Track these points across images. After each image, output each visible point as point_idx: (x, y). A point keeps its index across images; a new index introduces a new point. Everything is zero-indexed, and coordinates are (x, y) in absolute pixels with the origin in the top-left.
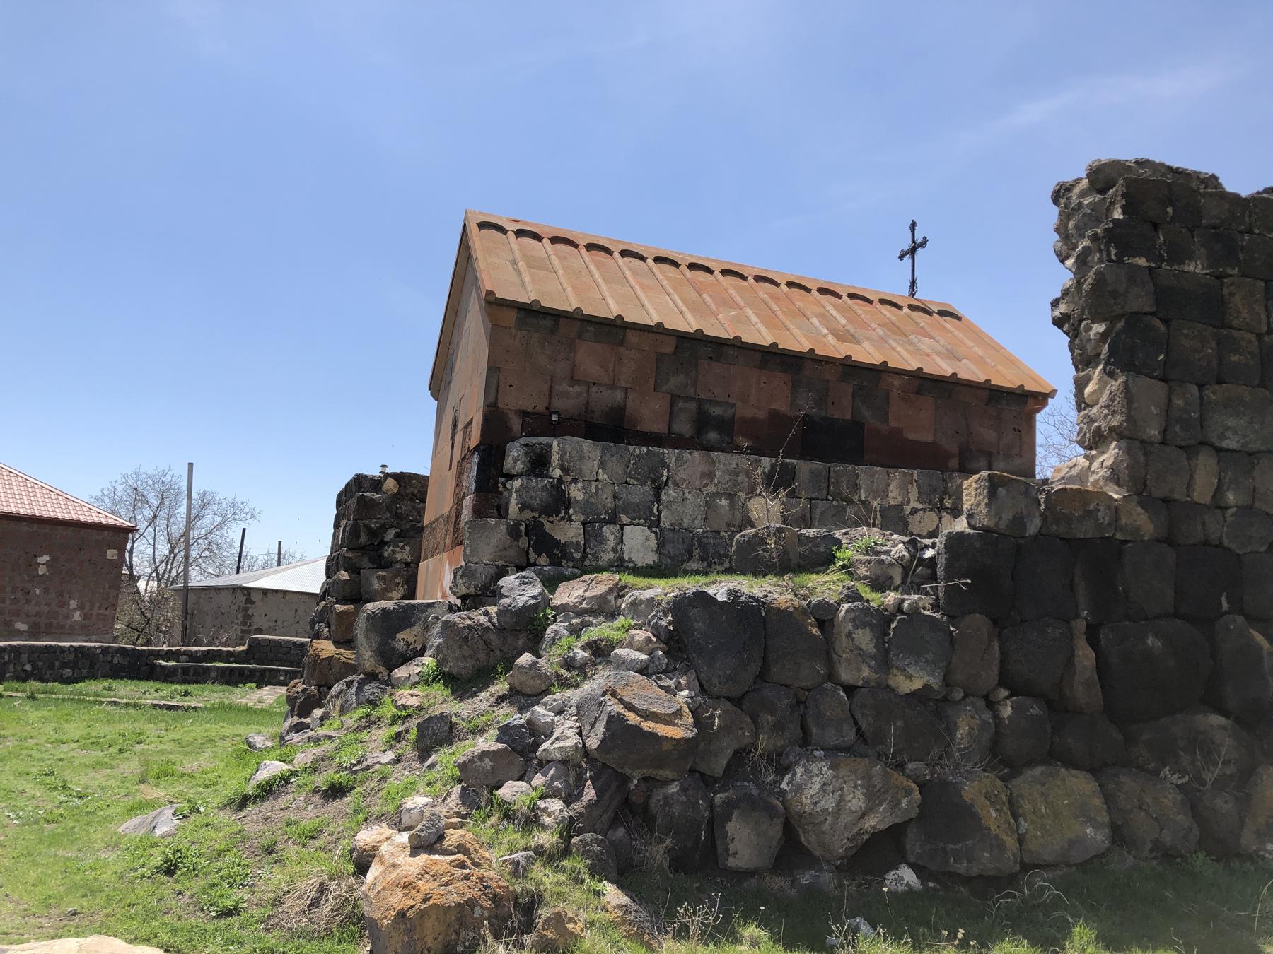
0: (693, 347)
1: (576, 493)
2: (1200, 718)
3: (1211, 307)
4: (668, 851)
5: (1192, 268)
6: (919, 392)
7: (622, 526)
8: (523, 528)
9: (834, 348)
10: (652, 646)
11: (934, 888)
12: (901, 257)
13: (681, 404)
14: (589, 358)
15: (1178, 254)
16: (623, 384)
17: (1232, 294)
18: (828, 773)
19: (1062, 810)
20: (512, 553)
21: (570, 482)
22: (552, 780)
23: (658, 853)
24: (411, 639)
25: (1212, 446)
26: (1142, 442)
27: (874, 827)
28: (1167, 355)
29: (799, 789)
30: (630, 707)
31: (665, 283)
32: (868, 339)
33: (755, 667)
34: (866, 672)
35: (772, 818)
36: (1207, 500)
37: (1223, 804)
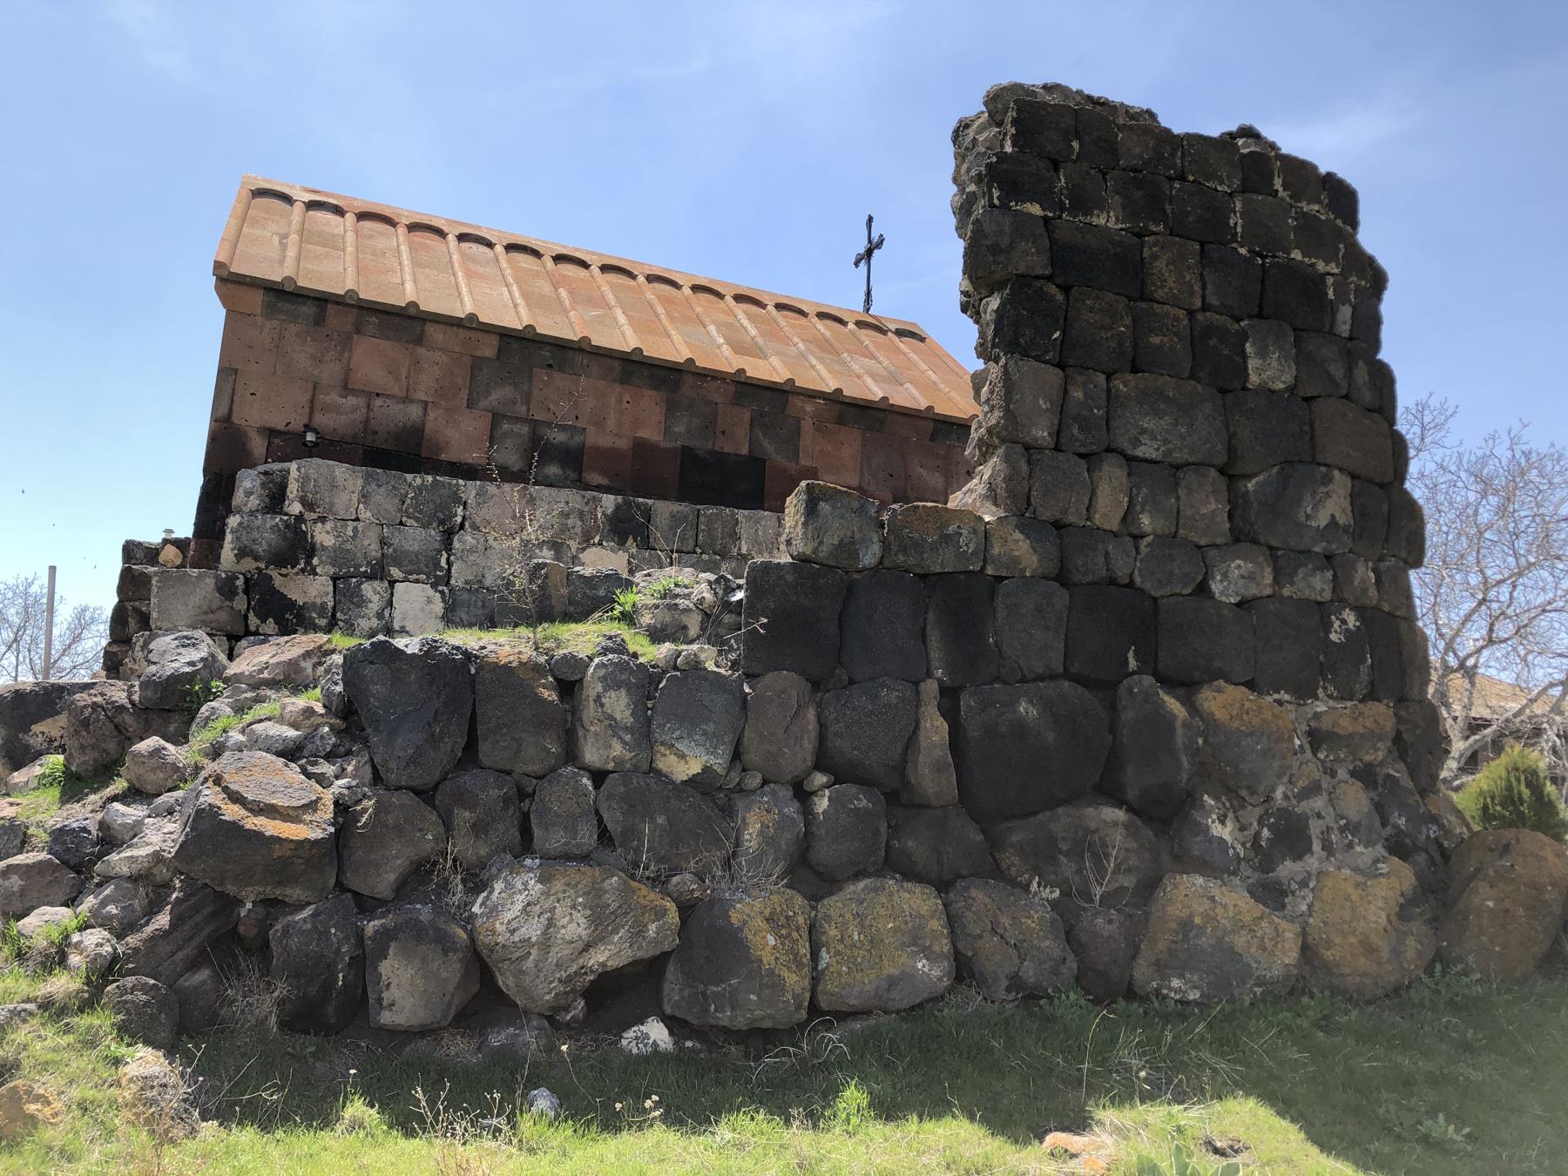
0: (523, 350)
1: (323, 536)
2: (1090, 811)
3: (1127, 272)
4: (281, 1003)
5: (1102, 221)
6: (840, 421)
7: (392, 583)
8: (240, 582)
9: (726, 360)
10: (315, 720)
11: (692, 1050)
12: (857, 264)
13: (506, 427)
14: (372, 360)
15: (1083, 203)
16: (422, 396)
17: (1154, 257)
18: (536, 888)
19: (889, 934)
20: (223, 616)
21: (315, 521)
22: (103, 904)
23: (260, 1003)
24: (55, 733)
25: (1122, 453)
26: (1027, 448)
27: (603, 964)
28: (1064, 333)
29: (494, 911)
30: (236, 798)
31: (508, 272)
32: (777, 353)
33: (454, 743)
34: (617, 749)
35: (445, 953)
36: (1114, 524)
37: (1103, 925)
